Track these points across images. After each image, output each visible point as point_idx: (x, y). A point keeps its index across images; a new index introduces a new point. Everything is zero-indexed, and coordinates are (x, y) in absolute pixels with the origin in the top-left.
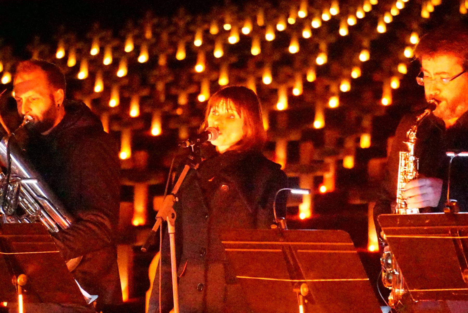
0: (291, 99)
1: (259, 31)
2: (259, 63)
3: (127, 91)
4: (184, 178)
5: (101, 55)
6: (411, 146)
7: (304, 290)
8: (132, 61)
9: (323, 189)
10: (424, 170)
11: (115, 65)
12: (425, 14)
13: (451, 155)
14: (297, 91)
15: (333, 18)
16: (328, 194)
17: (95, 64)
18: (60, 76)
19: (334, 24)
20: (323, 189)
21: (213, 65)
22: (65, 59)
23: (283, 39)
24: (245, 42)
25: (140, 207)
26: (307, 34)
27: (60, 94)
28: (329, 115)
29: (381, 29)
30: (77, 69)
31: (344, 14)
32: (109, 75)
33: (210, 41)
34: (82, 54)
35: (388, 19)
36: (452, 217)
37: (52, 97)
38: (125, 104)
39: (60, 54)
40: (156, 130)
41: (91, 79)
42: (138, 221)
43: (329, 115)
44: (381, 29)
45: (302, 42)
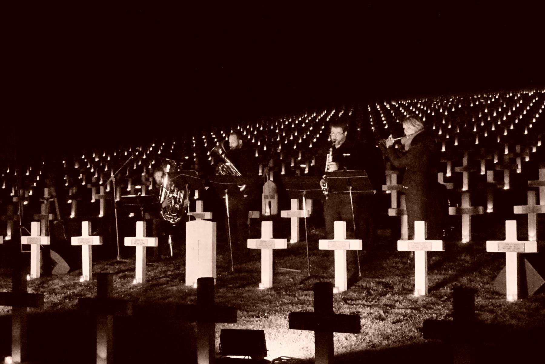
0: (303, 139)
1: (293, 121)
2: (294, 129)
3: (257, 138)
4: (396, 196)
5: (250, 128)
6: (331, 153)
7: (304, 193)
8: (258, 129)
9: (312, 165)
10: (334, 160)
11: (253, 131)
12: (340, 116)
13: (345, 155)
14: (305, 137)
15: (314, 117)
16: (313, 166)
17: (248, 131)
18: (239, 135)
19: (315, 118)
20: (312, 165)
21: (281, 131)
22: (240, 129)
23: (300, 123)
24: (290, 124)
25: (260, 171)
26: (307, 121)
27: (241, 141)
28: (313, 144)
29: (328, 120)
30: (243, 132)
31: (317, 115)
32: (252, 133)
33: (280, 124)
34: (245, 128)
35: (329, 117)
36: (345, 172)
37: (238, 143)
38: (256, 142)
39: (239, 128)
40: (261, 129)
41: (247, 135)
42: (260, 174)
43: (313, 144)
44: (328, 120)
45: (306, 124)
